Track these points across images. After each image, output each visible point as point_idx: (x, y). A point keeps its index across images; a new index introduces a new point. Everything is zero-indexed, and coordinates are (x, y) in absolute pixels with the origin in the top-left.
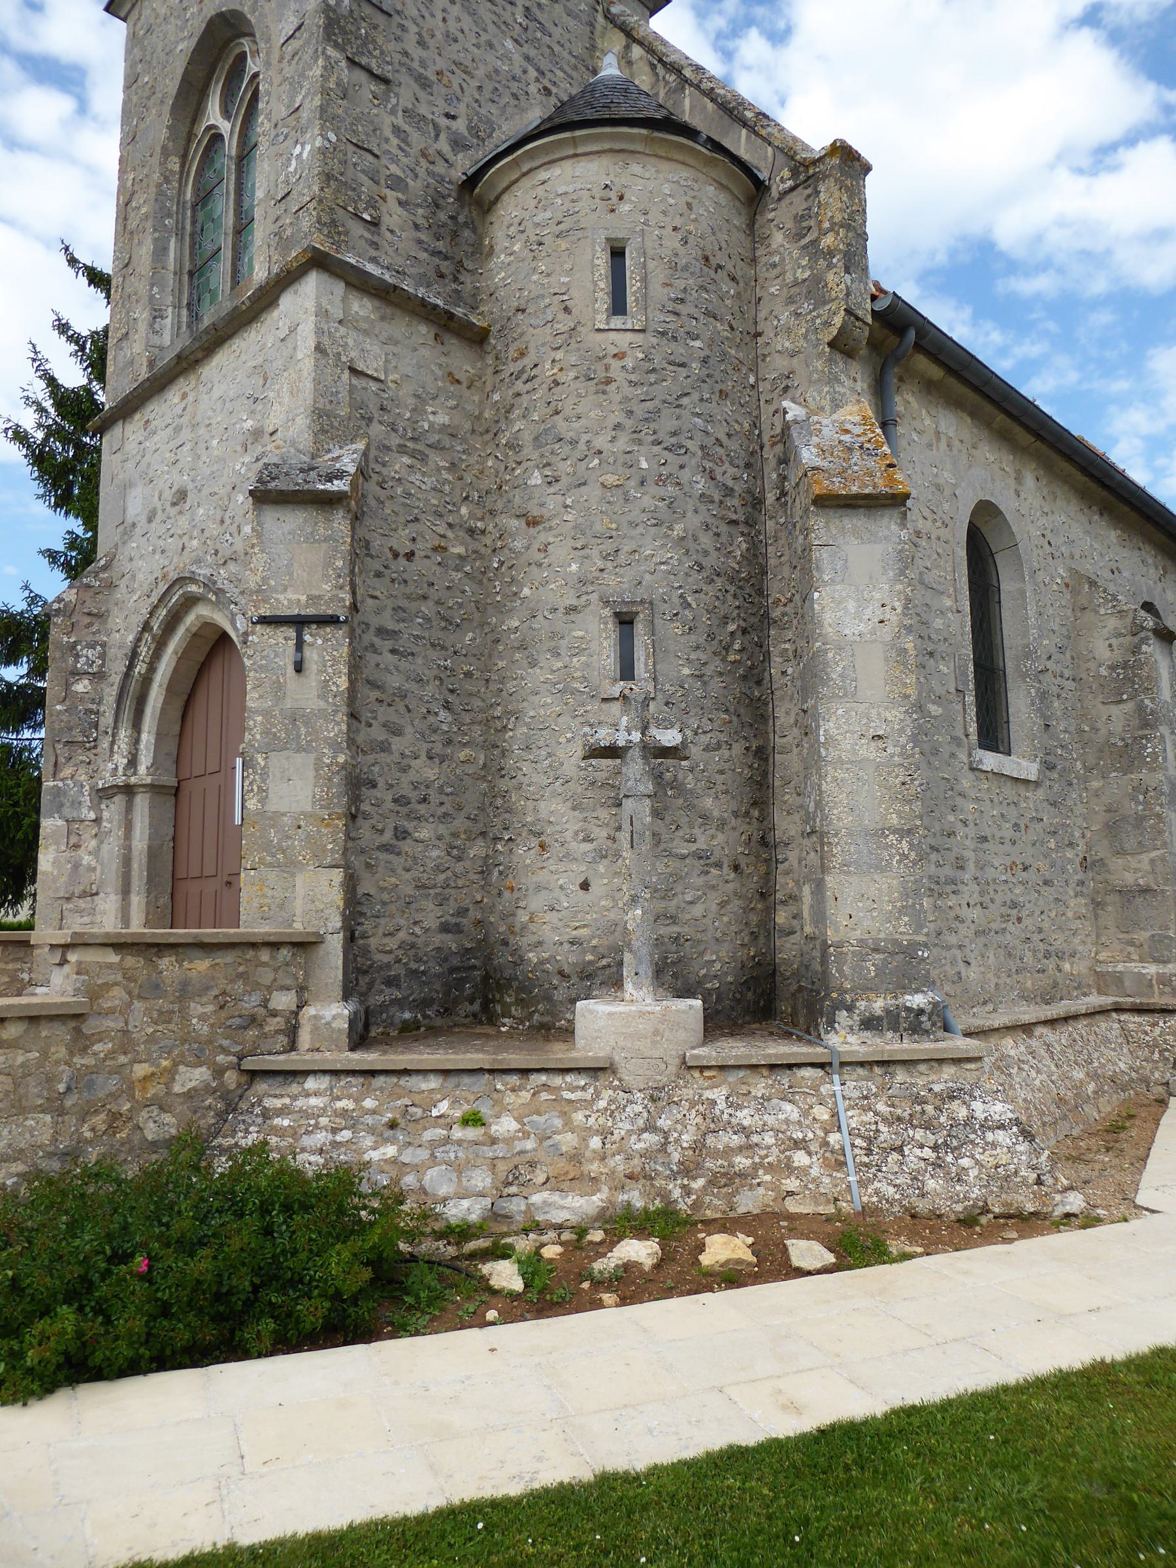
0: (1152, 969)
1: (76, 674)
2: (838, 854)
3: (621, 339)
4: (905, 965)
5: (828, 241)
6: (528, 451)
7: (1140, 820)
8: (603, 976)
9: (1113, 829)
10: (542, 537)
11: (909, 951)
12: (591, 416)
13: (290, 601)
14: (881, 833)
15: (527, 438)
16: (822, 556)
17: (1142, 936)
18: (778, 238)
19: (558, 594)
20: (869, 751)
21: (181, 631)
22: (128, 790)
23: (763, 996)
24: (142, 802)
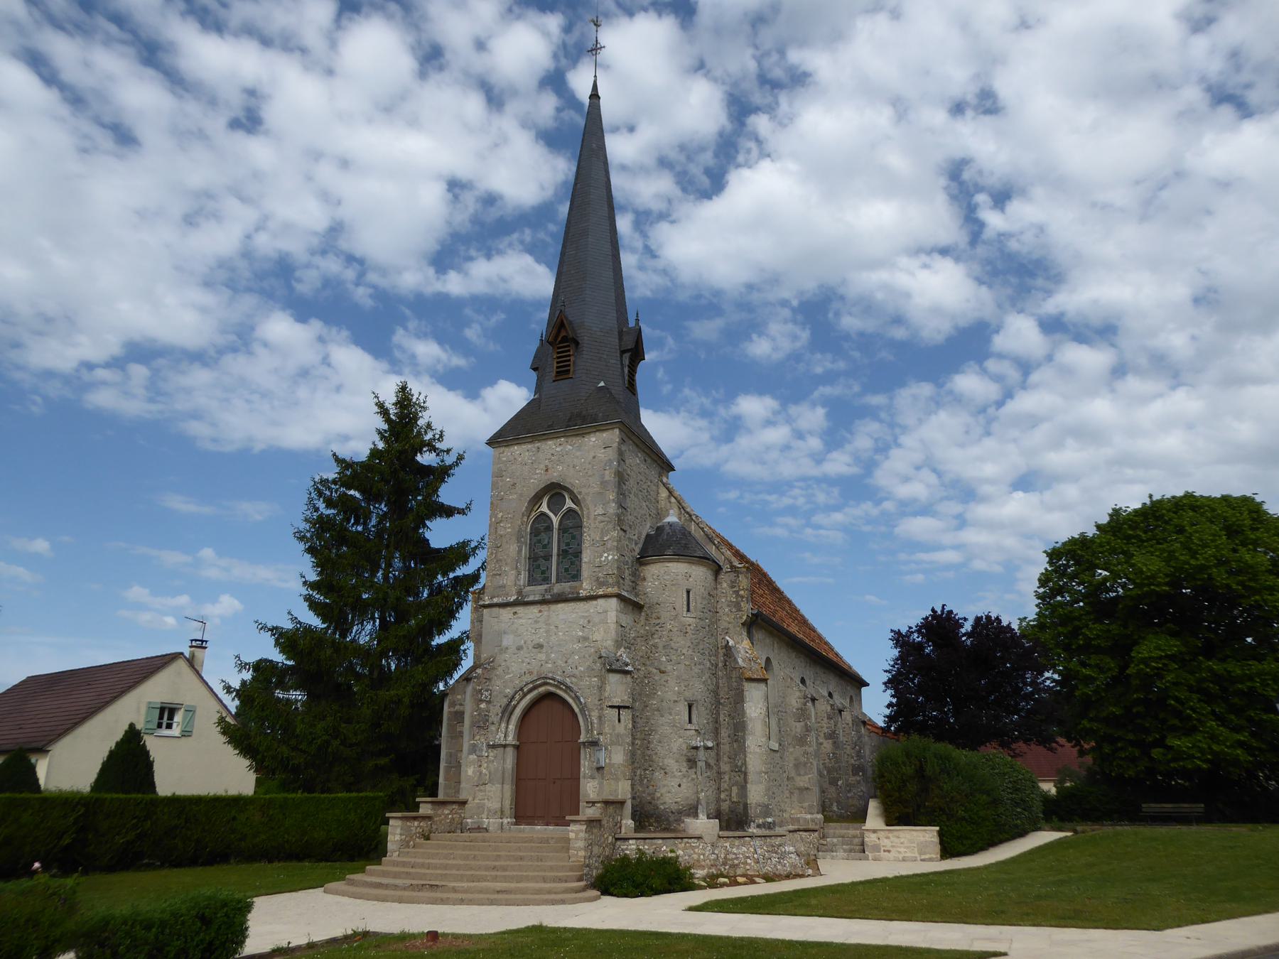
0: (809, 816)
1: (482, 701)
2: (751, 777)
3: (689, 619)
4: (767, 811)
5: (742, 593)
6: (660, 649)
7: (805, 764)
8: (693, 811)
9: (797, 766)
10: (665, 677)
11: (767, 806)
12: (681, 643)
13: (617, 701)
14: (761, 772)
15: (660, 645)
16: (746, 694)
17: (806, 805)
18: (725, 585)
19: (671, 696)
20: (758, 750)
21: (535, 692)
22: (505, 746)
23: (734, 820)
24: (510, 751)
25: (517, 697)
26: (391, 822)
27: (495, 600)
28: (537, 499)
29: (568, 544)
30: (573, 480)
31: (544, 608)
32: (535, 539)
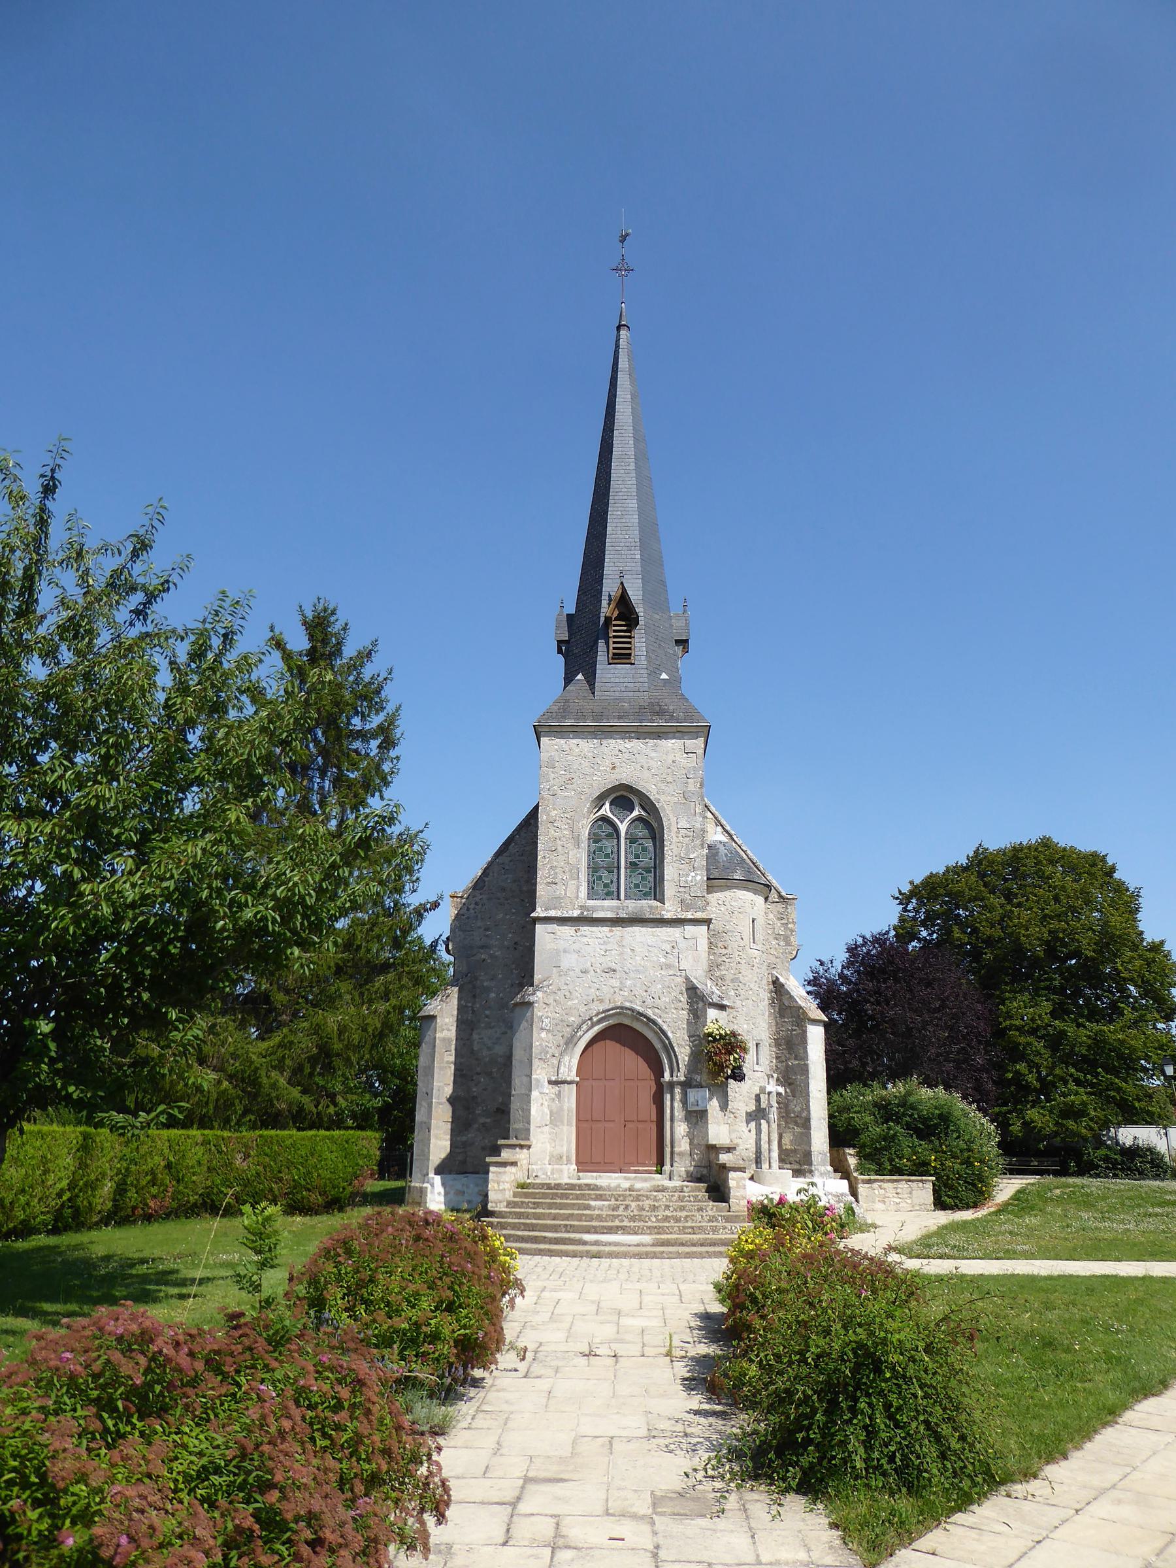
25: (585, 1027)
26: (492, 1169)
27: (552, 913)
28: (600, 800)
29: (637, 857)
30: (651, 789)
31: (618, 931)
32: (594, 847)
